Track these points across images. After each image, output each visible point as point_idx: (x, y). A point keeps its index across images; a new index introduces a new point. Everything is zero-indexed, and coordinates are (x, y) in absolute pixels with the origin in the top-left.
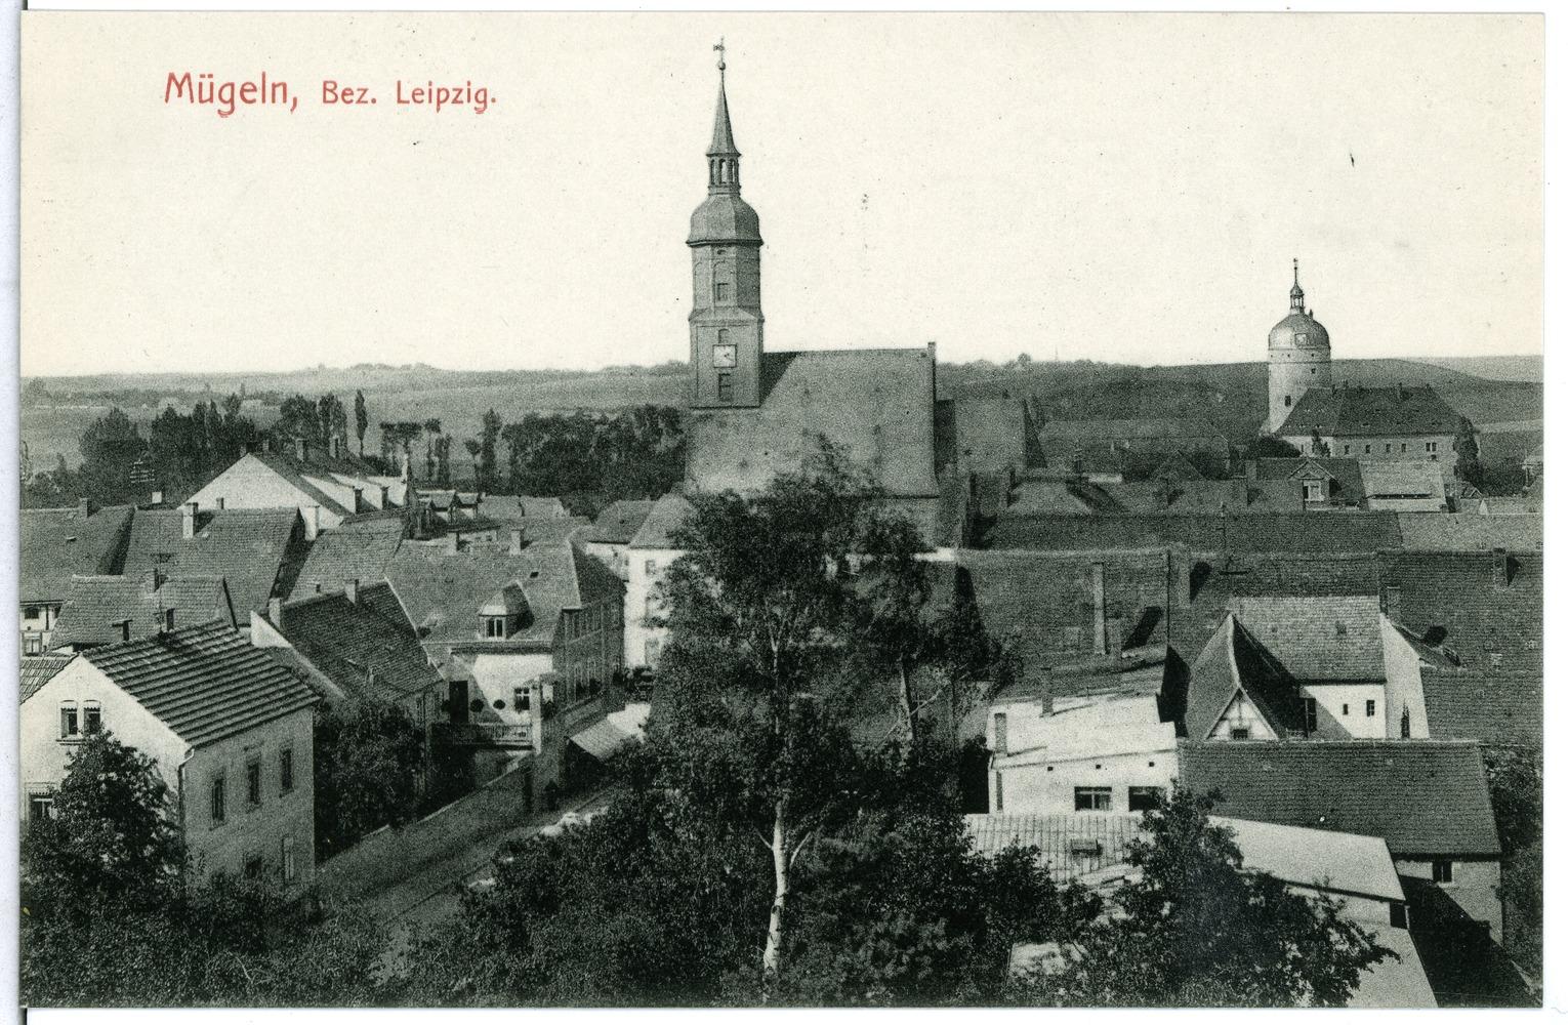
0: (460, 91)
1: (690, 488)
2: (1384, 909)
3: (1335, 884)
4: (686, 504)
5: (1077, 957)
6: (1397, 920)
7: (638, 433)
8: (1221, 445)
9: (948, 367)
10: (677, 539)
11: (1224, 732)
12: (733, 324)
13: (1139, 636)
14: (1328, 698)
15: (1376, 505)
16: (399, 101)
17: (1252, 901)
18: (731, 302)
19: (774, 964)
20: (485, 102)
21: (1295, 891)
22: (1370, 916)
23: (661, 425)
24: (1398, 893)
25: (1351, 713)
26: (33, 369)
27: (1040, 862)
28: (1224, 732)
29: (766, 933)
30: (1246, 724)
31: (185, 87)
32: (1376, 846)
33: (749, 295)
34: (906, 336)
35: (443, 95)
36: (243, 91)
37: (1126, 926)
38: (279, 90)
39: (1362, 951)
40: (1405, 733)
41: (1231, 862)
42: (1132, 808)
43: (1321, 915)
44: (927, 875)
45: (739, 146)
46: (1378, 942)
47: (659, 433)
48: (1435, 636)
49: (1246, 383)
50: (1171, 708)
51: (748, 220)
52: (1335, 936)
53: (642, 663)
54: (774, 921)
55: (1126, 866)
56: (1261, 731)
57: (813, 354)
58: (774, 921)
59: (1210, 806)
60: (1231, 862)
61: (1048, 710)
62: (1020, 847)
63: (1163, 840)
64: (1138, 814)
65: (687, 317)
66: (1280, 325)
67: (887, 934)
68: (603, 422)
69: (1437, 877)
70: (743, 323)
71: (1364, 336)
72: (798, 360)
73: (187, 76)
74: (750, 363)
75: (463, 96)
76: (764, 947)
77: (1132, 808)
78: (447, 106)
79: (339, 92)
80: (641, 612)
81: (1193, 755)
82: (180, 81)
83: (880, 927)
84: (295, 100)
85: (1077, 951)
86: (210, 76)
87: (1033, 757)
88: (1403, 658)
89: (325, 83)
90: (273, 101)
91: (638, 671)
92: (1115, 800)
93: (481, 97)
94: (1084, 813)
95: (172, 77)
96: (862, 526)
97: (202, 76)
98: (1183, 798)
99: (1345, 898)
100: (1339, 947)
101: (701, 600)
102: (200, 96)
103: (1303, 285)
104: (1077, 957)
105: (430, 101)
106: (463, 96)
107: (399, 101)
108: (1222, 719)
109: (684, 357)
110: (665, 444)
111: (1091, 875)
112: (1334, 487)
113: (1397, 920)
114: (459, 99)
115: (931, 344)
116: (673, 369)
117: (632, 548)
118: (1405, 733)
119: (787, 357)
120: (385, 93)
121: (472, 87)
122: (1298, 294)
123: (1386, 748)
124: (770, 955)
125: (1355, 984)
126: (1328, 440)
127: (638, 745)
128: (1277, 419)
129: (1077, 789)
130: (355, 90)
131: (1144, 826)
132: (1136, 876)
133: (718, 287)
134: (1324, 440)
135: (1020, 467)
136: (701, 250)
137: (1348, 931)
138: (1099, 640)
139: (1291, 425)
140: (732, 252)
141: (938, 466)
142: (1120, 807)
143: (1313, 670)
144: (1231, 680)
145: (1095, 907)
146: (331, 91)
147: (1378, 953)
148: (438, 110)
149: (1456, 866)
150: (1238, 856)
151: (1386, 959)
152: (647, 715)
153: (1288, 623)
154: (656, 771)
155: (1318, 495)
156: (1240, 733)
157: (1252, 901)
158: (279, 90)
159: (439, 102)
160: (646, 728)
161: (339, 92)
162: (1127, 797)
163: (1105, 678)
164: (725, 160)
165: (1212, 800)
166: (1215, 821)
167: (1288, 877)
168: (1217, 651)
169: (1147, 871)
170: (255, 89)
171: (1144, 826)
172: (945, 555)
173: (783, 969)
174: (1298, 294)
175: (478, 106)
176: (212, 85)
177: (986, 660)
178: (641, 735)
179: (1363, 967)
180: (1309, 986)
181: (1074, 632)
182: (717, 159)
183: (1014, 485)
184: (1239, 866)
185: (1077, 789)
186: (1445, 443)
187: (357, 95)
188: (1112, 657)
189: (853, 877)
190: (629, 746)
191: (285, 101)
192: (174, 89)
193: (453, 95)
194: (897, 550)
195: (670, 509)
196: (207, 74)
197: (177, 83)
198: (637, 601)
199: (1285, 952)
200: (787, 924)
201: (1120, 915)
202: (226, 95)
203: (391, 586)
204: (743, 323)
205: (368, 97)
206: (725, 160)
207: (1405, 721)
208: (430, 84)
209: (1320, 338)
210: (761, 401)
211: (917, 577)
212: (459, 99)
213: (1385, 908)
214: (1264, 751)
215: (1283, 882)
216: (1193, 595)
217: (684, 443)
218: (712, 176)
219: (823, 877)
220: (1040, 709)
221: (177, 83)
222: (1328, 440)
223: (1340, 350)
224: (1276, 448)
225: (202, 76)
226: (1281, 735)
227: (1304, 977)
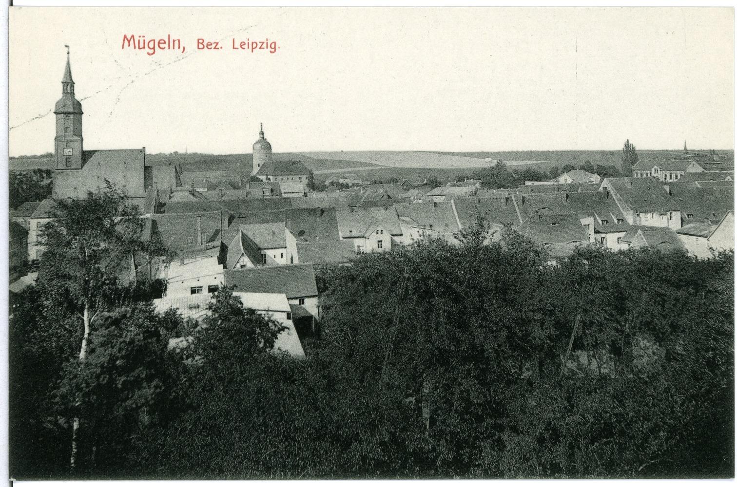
0: (263, 43)
1: (54, 196)
2: (285, 315)
3: (270, 309)
4: (52, 202)
5: (190, 341)
6: (289, 318)
7: (34, 178)
8: (238, 179)
9: (150, 155)
10: (49, 214)
11: (238, 266)
12: (71, 141)
13: (212, 239)
14: (270, 253)
15: (284, 196)
17: (246, 317)
18: (71, 133)
19: (84, 357)
20: (275, 48)
21: (259, 312)
22: (281, 318)
23: (45, 175)
24: (289, 310)
25: (277, 257)
27: (179, 312)
28: (238, 266)
29: (81, 347)
30: (245, 263)
31: (132, 42)
32: (283, 297)
33: (78, 133)
34: (134, 144)
35: (255, 45)
36: (159, 43)
37: (207, 330)
38: (177, 43)
39: (279, 328)
40: (292, 262)
41: (240, 306)
42: (209, 292)
43: (266, 319)
44: (140, 320)
45: (74, 79)
46: (283, 325)
47: (43, 178)
48: (302, 233)
49: (244, 160)
50: (222, 260)
51: (78, 105)
52: (270, 324)
53: (35, 258)
54: (84, 343)
55: (208, 310)
56: (249, 265)
57: (101, 151)
58: (84, 343)
59: (233, 289)
60: (240, 306)
61: (183, 263)
62: (173, 308)
63: (218, 301)
64: (211, 294)
65: (54, 138)
66: (257, 142)
67: (124, 342)
68: (20, 174)
69: (300, 304)
70: (77, 141)
71: (281, 146)
72: (96, 153)
73: (133, 36)
74: (78, 153)
75: (264, 46)
76: (80, 351)
77: (209, 292)
78: (257, 50)
79: (205, 44)
80: (35, 240)
81: (229, 274)
82: (129, 39)
83: (122, 340)
84: (184, 48)
85: (191, 339)
86: (144, 37)
87: (177, 279)
88: (291, 240)
89: (198, 40)
90: (174, 48)
91: (33, 261)
92: (203, 291)
93: (273, 46)
94: (194, 295)
95: (125, 37)
96: (120, 209)
97: (140, 37)
98: (224, 288)
99: (274, 312)
100: (271, 328)
101: (58, 235)
103: (263, 130)
104: (190, 341)
105: (248, 48)
106: (264, 46)
107: (234, 48)
108: (238, 262)
109: (52, 150)
110: (46, 182)
111: (195, 315)
112: (272, 191)
113: (289, 318)
114: (262, 47)
115: (144, 148)
116: (49, 155)
117: (32, 218)
118: (292, 262)
119: (91, 153)
120: (227, 44)
123: (287, 267)
124: (82, 354)
125: (277, 338)
126: (271, 177)
127: (33, 287)
128: (256, 170)
129: (192, 288)
131: (212, 297)
132: (210, 313)
133: (66, 129)
134: (269, 177)
135: (174, 187)
136: (59, 115)
137: (274, 322)
138: (199, 241)
139: (260, 172)
140: (72, 116)
141: (146, 187)
142: (205, 292)
143: (266, 245)
144: (240, 250)
145: (196, 325)
146: (202, 43)
147: (283, 329)
148: (252, 52)
149: (306, 300)
150: (241, 303)
151: (286, 330)
152: (37, 276)
153: (258, 232)
154: (40, 296)
155: (268, 193)
156: (243, 266)
157: (246, 317)
159: (253, 49)
160: (36, 281)
161: (205, 44)
162: (207, 288)
163: (204, 252)
164: (69, 84)
165: (234, 287)
166: (235, 294)
167: (257, 308)
168: (235, 244)
169: (213, 311)
170: (165, 43)
171: (212, 297)
172: (148, 215)
173: (87, 358)
174: (262, 133)
175: (271, 50)
176: (144, 40)
177: (160, 250)
178: (34, 283)
179: (279, 333)
180: (263, 341)
181: (190, 239)
182: (66, 84)
183: (172, 193)
184: (242, 307)
185: (192, 288)
186: (304, 177)
187: (214, 45)
188: (203, 246)
189: (112, 324)
190: (30, 287)
191: (179, 48)
192: (126, 43)
194: (132, 217)
195: (46, 204)
196: (142, 35)
197: (128, 40)
198: (33, 237)
199: (255, 331)
200: (89, 342)
201: (205, 326)
202: (151, 45)
204: (77, 141)
206: (69, 84)
207: (292, 259)
209: (268, 147)
210: (82, 166)
211: (141, 225)
212: (262, 47)
213: (286, 314)
214: (250, 270)
215: (255, 310)
216: (230, 223)
217: (52, 181)
218: (64, 89)
219: (101, 326)
220: (180, 264)
221: (127, 39)
222: (271, 177)
223: (274, 150)
224: (255, 179)
225: (140, 37)
226: (255, 266)
227: (262, 338)
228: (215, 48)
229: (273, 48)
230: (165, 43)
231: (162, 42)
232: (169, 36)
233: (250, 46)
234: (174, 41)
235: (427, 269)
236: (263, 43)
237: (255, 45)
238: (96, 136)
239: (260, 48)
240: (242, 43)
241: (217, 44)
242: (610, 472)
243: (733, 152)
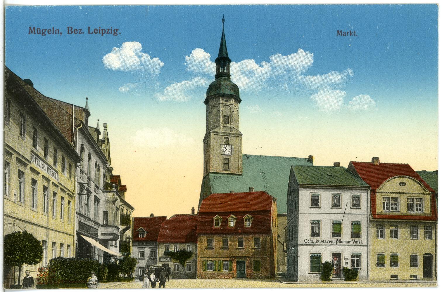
0: (109, 30)
79: (73, 30)
106: (110, 31)
114: (109, 32)
116: (370, 162)
159: (102, 33)
161: (73, 30)
164: (223, 35)
187: (78, 31)
193: (106, 31)
208: (100, 28)
229: (339, 33)
230: (97, 30)
231: (96, 30)
232: (89, 28)
233: (113, 32)
234: (56, 30)
235: (134, 7)
237: (104, 31)
239: (107, 33)
240: (95, 29)
241: (81, 30)
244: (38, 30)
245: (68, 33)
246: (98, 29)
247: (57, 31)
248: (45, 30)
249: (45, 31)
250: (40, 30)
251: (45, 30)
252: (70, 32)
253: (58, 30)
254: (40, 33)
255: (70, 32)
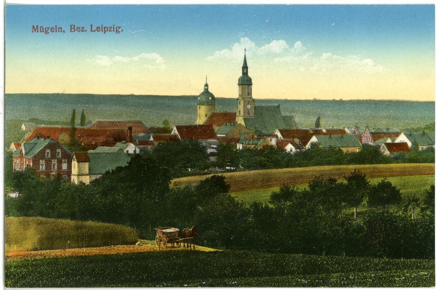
0: (111, 27)
16: (92, 31)
26: (10, 91)
45: (248, 65)
102: (41, 30)
114: (82, 28)
121: (115, 26)
122: (206, 85)
130: (81, 28)
146: (74, 28)
158: (60, 29)
161: (76, 28)
164: (245, 67)
174: (206, 85)
187: (81, 29)
193: (109, 29)
203: (101, 120)
205: (84, 29)
206: (245, 67)
208: (102, 25)
228: (82, 31)
230: (54, 29)
231: (78, 28)
236: (111, 27)
237: (106, 29)
238: (258, 92)
240: (78, 27)
241: (84, 28)
242: (250, 286)
243: (429, 106)
244: (42, 28)
245: (71, 31)
246: (101, 27)
247: (60, 29)
248: (48, 28)
249: (48, 29)
250: (43, 28)
251: (48, 28)
252: (73, 30)
253: (61, 28)
254: (43, 31)
255: (73, 30)
